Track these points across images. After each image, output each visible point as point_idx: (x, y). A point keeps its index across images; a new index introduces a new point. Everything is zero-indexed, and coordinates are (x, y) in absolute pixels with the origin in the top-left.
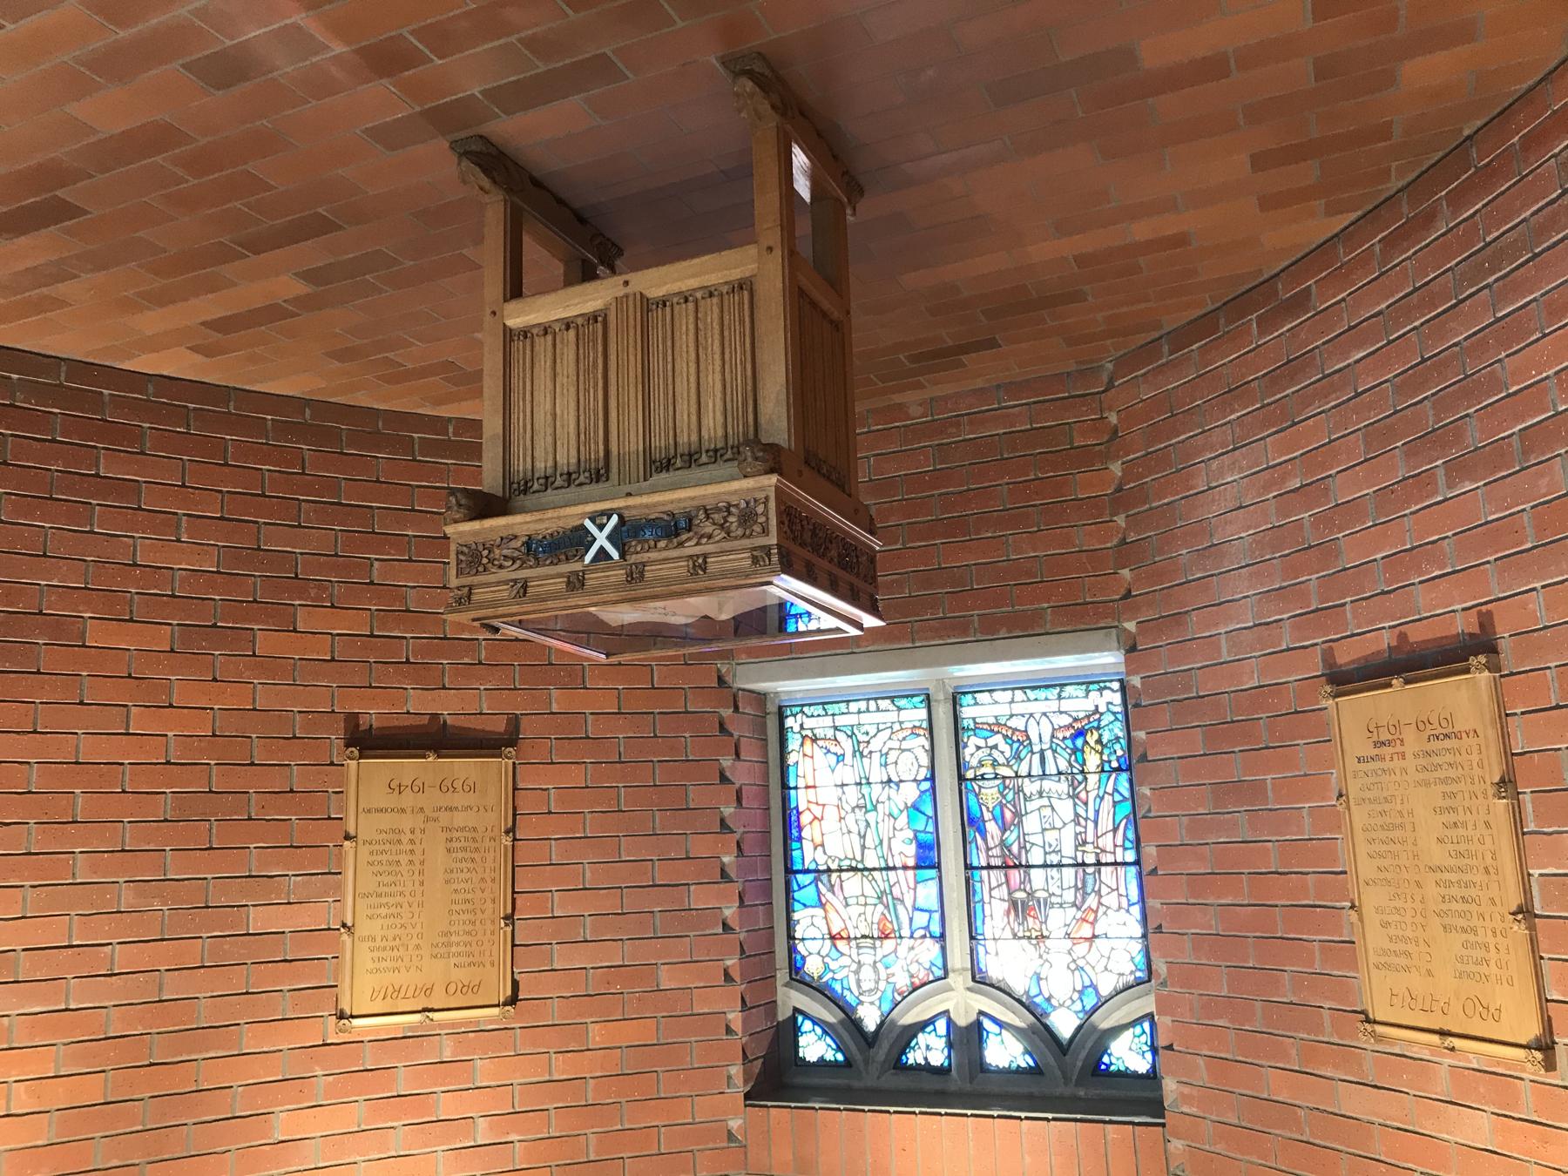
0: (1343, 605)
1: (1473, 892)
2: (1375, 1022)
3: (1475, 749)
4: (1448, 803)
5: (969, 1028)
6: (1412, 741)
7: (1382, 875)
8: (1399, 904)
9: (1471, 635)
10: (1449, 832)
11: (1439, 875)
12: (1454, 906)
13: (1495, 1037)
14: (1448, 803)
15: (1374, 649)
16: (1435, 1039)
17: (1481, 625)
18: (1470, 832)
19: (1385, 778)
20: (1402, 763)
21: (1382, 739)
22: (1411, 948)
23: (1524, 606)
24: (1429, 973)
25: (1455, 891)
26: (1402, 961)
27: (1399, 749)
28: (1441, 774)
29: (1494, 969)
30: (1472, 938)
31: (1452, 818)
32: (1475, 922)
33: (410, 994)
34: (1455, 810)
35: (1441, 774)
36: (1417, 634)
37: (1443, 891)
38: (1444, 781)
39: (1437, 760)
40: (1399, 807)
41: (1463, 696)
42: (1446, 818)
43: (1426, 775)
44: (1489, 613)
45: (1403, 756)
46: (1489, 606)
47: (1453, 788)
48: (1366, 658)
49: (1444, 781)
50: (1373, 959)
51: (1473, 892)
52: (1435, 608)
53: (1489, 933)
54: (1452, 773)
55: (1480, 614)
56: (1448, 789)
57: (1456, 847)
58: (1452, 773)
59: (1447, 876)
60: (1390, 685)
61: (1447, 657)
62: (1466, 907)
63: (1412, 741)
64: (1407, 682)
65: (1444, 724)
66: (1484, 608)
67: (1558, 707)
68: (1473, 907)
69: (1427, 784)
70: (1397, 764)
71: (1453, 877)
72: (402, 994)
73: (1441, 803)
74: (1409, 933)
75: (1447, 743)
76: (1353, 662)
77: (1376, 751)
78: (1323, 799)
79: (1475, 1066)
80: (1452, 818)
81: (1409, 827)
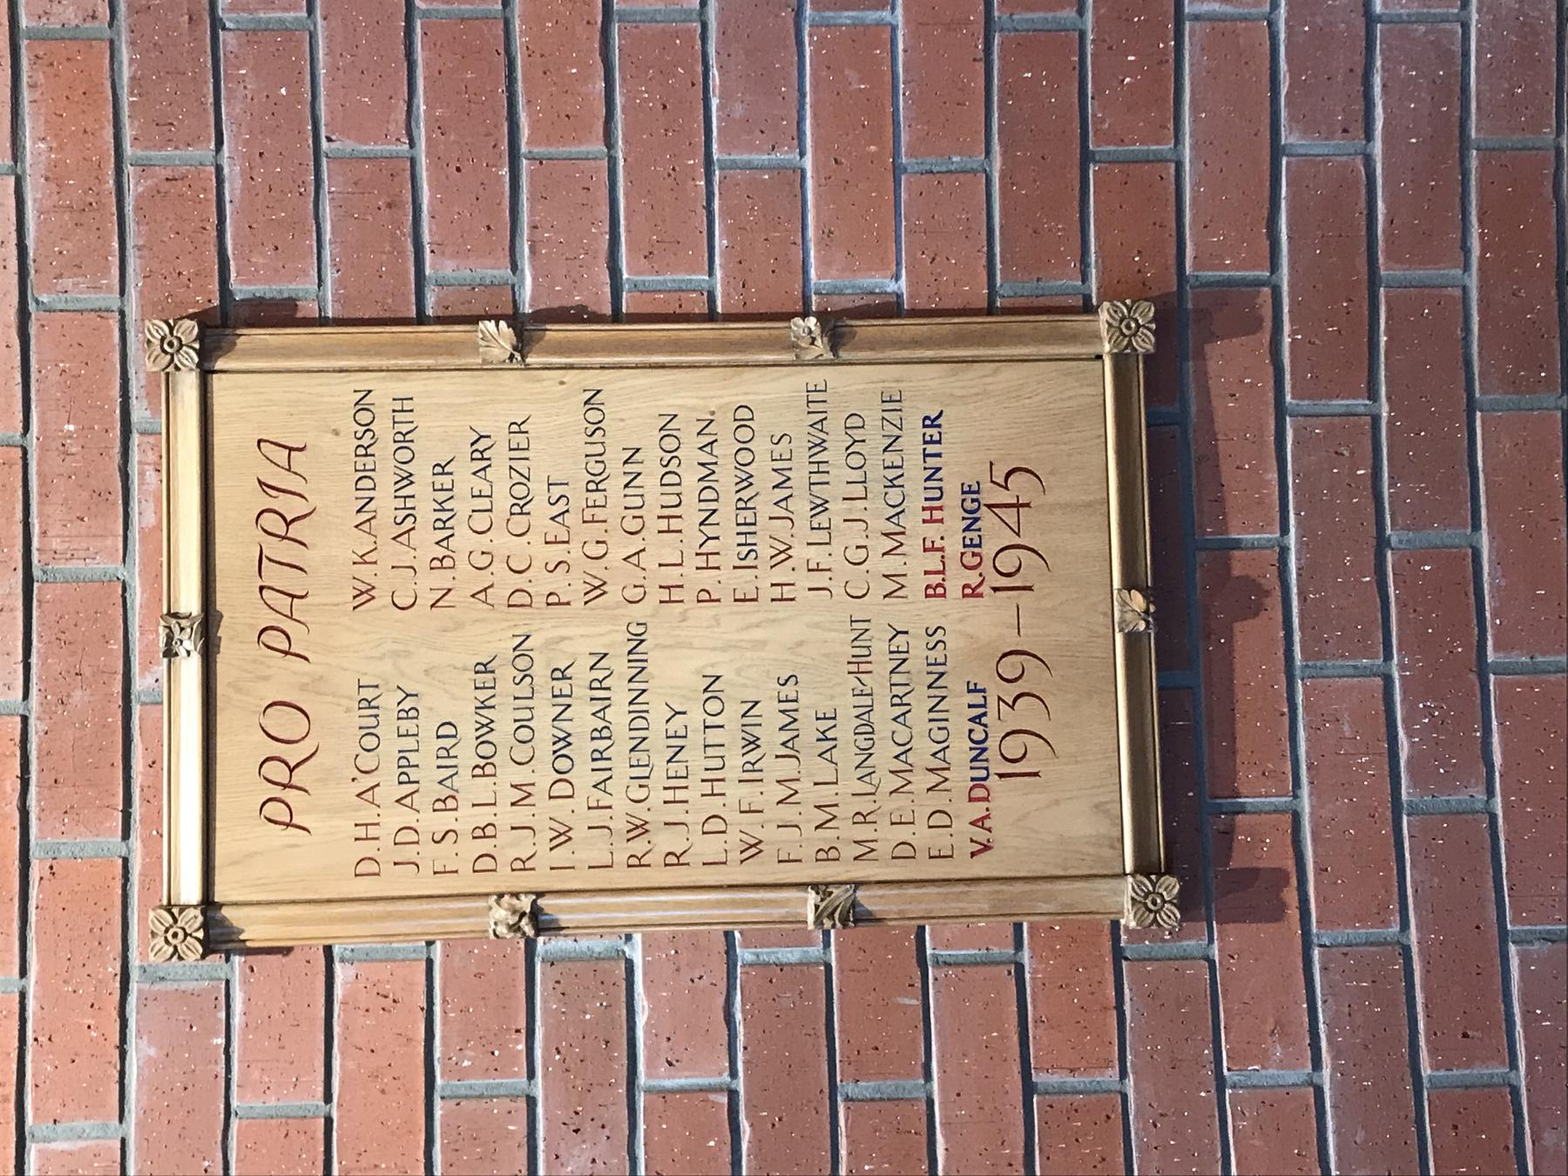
0: (1373, 395)
1: (583, 776)
2: (206, 374)
3: (941, 840)
4: (808, 730)
5: (214, 952)
6: (978, 624)
7: (614, 458)
8: (540, 510)
9: (1229, 833)
10: (732, 716)
11: (620, 666)
12: (544, 712)
13: (219, 824)
14: (808, 730)
15: (1234, 494)
16: (189, 601)
17: (1251, 875)
18: (735, 792)
19: (876, 512)
20: (917, 583)
21: (987, 519)
22: (425, 540)
23: (1281, 1029)
24: (365, 594)
25: (582, 719)
26: (386, 503)
27: (957, 579)
28: (883, 714)
29: (397, 817)
30: (466, 755)
31: (771, 738)
32: (509, 774)
33: (273, 575)
34: (789, 750)
35: (883, 714)
36: (1252, 649)
37: (582, 674)
38: (866, 728)
39: (920, 702)
40: (800, 552)
41: (1080, 801)
42: (770, 718)
43: (881, 663)
44: (1276, 913)
45: (935, 592)
46: (1294, 913)
47: (847, 755)
48: (1212, 459)
49: (866, 728)
50: (385, 390)
51: (583, 776)
52: (1312, 728)
53: (484, 816)
54: (884, 755)
55: (1280, 877)
56: (844, 731)
57: (696, 738)
58: (884, 755)
59: (621, 695)
60: (1129, 584)
61: (1191, 837)
62: (544, 747)
63: (978, 624)
64: (1132, 640)
65: (1013, 747)
66: (1291, 896)
67: (1029, 1089)
68: (543, 776)
69: (859, 664)
70: (916, 565)
71: (619, 715)
72: (275, 549)
73: (810, 701)
74: (463, 540)
75: (960, 750)
76: (1208, 414)
77: (953, 498)
78: (826, 235)
79: (138, 684)
80: (771, 738)
81: (744, 582)
